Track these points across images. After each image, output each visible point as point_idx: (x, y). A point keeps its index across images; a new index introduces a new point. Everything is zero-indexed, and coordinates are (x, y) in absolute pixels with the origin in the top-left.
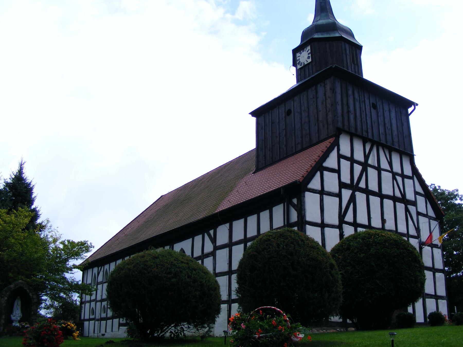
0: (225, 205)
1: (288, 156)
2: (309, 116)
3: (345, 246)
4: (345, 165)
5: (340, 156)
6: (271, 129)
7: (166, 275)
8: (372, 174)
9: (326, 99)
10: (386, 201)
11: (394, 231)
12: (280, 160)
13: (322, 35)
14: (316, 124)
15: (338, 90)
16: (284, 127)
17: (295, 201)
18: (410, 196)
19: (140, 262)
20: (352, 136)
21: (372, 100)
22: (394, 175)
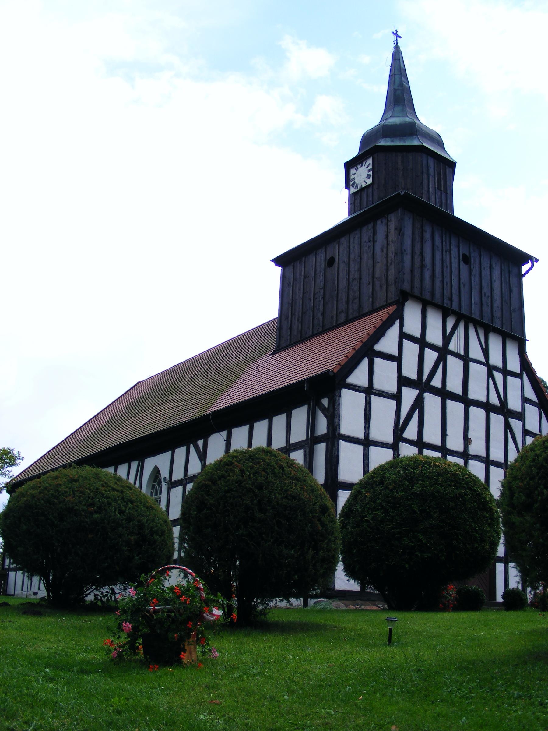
0: (224, 402)
1: (325, 330)
2: (360, 270)
3: (377, 478)
4: (411, 350)
5: (403, 336)
6: (302, 287)
7: (85, 508)
8: (454, 366)
9: (388, 244)
10: (473, 410)
11: (483, 457)
12: (313, 336)
13: (392, 141)
14: (369, 283)
15: (408, 231)
16: (322, 285)
17: (325, 402)
18: (514, 404)
19: (51, 485)
20: (426, 305)
21: (464, 250)
22: (491, 369)
